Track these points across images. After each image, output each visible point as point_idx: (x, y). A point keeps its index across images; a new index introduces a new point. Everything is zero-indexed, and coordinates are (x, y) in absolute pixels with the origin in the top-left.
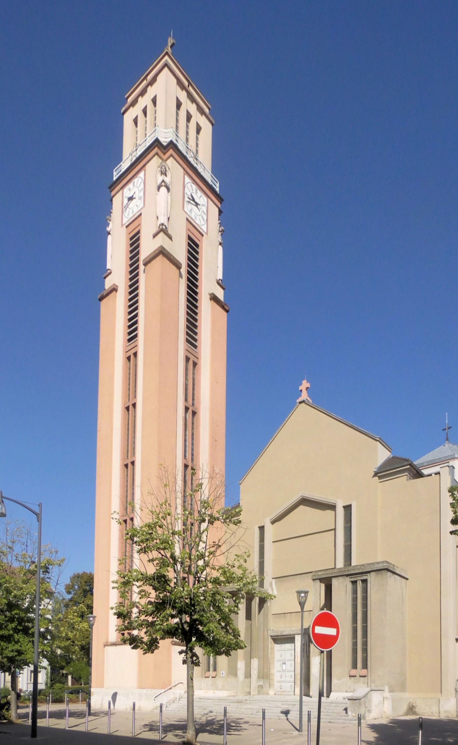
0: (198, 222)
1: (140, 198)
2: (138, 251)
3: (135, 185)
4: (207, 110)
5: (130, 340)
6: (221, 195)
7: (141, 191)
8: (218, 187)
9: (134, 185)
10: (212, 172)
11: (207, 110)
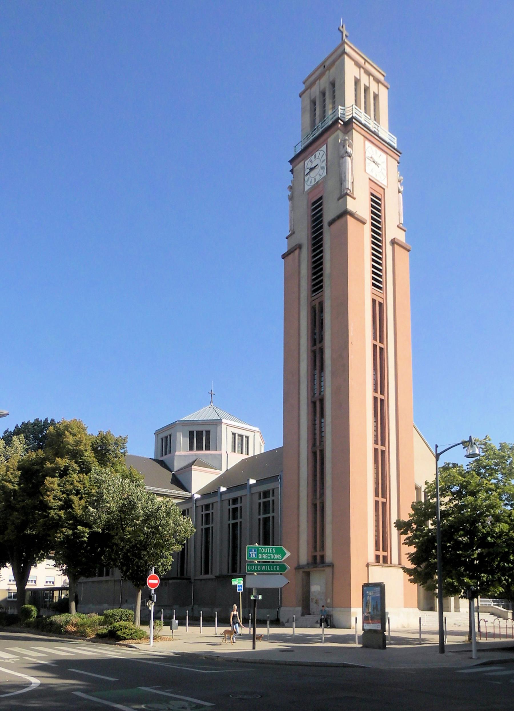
0: (378, 179)
1: (322, 168)
2: (322, 214)
3: (317, 157)
4: (382, 78)
5: (314, 291)
6: (398, 149)
7: (323, 161)
8: (396, 142)
9: (315, 157)
10: (389, 131)
11: (382, 78)
